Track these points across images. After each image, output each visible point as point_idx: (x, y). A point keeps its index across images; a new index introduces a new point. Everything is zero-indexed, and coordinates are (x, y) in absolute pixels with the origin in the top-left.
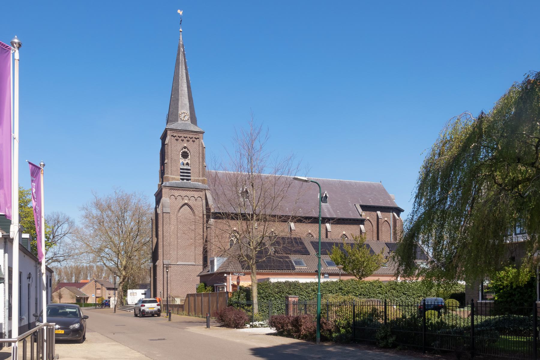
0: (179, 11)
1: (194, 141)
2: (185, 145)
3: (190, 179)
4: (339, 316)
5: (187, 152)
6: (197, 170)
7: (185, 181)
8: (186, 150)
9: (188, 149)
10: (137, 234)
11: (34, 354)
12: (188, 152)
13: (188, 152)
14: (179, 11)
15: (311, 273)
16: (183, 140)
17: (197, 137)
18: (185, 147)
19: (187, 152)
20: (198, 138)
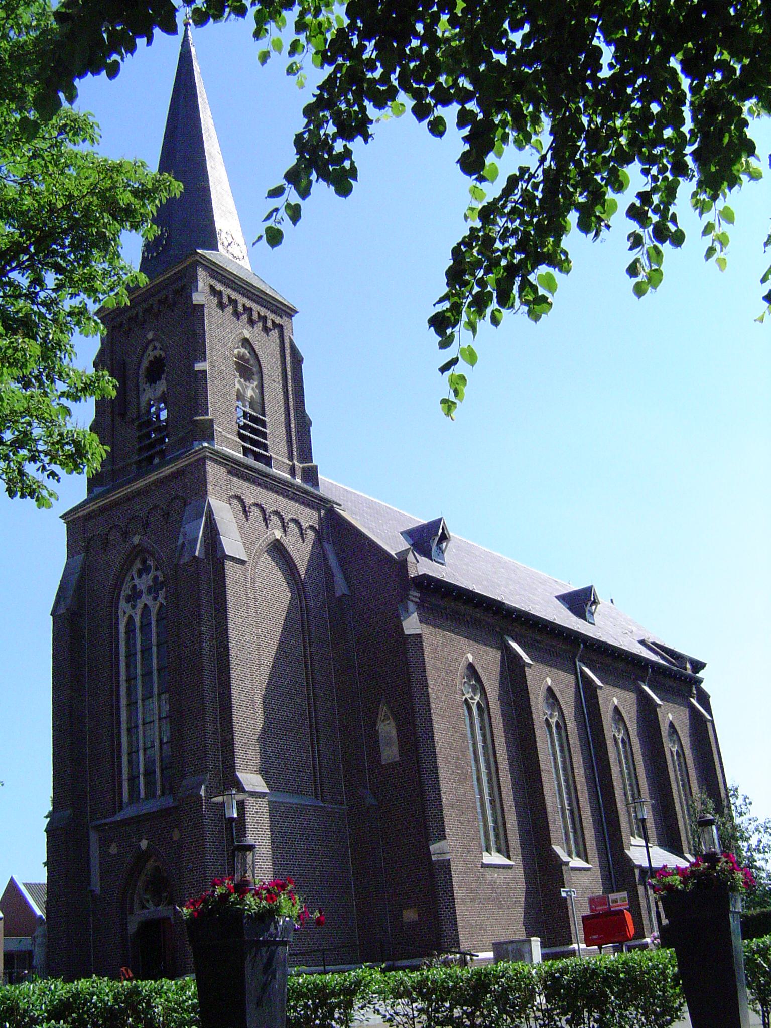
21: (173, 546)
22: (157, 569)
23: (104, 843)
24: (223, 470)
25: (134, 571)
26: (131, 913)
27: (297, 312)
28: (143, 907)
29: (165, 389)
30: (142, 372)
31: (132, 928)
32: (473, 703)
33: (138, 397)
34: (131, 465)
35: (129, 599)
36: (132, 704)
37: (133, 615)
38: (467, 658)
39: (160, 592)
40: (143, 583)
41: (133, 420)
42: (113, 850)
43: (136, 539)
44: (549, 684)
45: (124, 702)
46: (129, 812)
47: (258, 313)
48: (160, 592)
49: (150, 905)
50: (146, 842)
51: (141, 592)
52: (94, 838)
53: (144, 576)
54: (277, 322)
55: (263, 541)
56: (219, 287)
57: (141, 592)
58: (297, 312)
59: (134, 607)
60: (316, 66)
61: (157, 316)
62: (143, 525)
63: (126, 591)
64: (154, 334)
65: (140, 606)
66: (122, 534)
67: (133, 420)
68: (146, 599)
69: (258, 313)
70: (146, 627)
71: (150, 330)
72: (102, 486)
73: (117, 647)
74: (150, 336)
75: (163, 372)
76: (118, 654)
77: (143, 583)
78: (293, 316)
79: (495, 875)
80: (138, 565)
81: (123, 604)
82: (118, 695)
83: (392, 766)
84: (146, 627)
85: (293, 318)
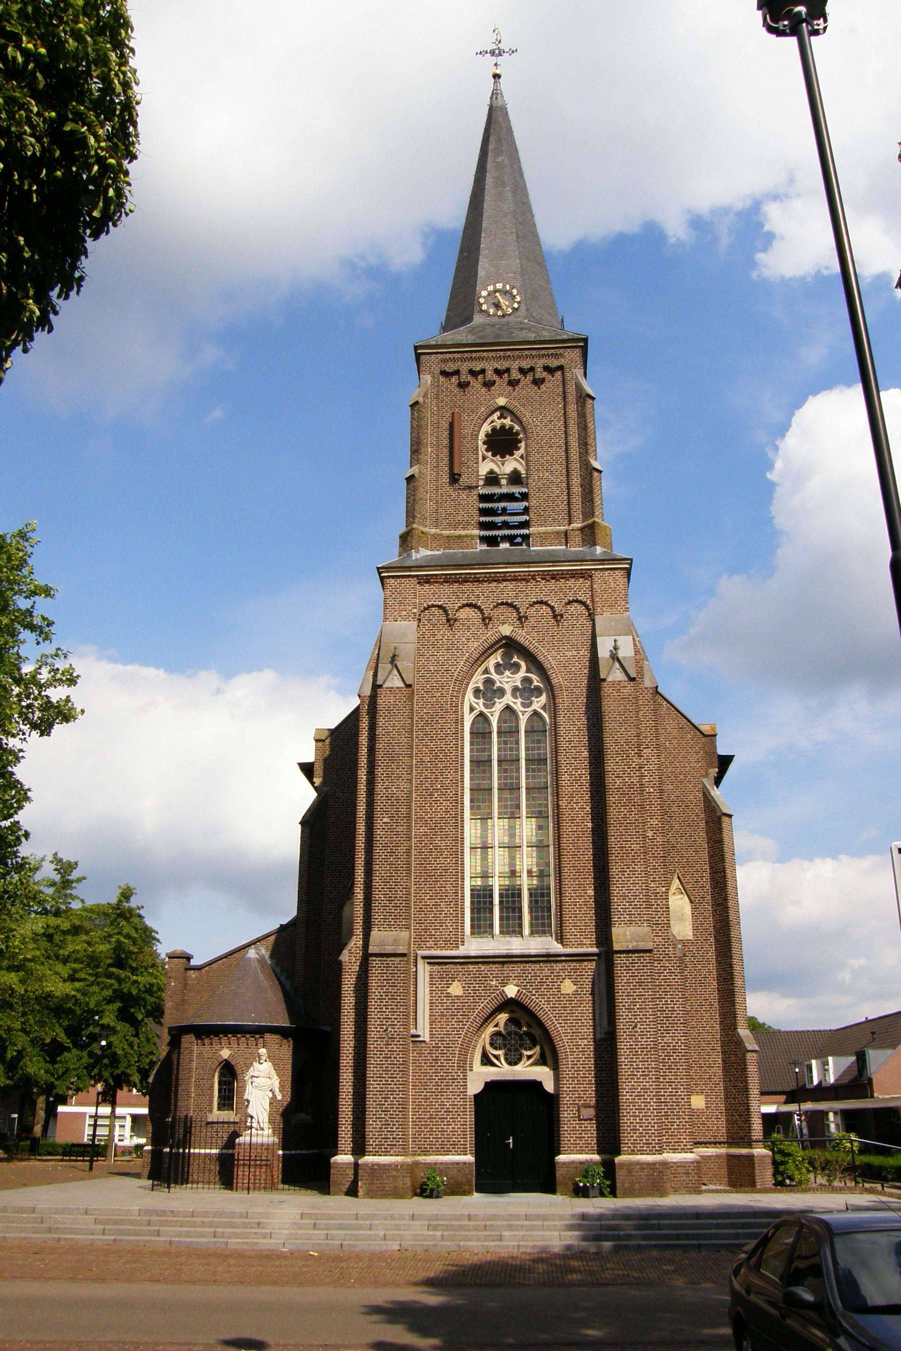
0: (93, 188)
1: (538, 382)
2: (501, 401)
3: (526, 538)
4: (636, 1027)
5: (512, 428)
6: (558, 491)
7: (504, 546)
8: (508, 422)
9: (517, 419)
10: (289, 1345)
11: (352, 1015)
12: (517, 428)
13: (517, 428)
14: (93, 188)
15: (248, 1033)
16: (488, 385)
17: (554, 363)
18: (504, 411)
19: (512, 428)
20: (561, 368)
23: (439, 982)
30: (482, 436)
46: (474, 946)
50: (517, 988)
63: (478, 680)
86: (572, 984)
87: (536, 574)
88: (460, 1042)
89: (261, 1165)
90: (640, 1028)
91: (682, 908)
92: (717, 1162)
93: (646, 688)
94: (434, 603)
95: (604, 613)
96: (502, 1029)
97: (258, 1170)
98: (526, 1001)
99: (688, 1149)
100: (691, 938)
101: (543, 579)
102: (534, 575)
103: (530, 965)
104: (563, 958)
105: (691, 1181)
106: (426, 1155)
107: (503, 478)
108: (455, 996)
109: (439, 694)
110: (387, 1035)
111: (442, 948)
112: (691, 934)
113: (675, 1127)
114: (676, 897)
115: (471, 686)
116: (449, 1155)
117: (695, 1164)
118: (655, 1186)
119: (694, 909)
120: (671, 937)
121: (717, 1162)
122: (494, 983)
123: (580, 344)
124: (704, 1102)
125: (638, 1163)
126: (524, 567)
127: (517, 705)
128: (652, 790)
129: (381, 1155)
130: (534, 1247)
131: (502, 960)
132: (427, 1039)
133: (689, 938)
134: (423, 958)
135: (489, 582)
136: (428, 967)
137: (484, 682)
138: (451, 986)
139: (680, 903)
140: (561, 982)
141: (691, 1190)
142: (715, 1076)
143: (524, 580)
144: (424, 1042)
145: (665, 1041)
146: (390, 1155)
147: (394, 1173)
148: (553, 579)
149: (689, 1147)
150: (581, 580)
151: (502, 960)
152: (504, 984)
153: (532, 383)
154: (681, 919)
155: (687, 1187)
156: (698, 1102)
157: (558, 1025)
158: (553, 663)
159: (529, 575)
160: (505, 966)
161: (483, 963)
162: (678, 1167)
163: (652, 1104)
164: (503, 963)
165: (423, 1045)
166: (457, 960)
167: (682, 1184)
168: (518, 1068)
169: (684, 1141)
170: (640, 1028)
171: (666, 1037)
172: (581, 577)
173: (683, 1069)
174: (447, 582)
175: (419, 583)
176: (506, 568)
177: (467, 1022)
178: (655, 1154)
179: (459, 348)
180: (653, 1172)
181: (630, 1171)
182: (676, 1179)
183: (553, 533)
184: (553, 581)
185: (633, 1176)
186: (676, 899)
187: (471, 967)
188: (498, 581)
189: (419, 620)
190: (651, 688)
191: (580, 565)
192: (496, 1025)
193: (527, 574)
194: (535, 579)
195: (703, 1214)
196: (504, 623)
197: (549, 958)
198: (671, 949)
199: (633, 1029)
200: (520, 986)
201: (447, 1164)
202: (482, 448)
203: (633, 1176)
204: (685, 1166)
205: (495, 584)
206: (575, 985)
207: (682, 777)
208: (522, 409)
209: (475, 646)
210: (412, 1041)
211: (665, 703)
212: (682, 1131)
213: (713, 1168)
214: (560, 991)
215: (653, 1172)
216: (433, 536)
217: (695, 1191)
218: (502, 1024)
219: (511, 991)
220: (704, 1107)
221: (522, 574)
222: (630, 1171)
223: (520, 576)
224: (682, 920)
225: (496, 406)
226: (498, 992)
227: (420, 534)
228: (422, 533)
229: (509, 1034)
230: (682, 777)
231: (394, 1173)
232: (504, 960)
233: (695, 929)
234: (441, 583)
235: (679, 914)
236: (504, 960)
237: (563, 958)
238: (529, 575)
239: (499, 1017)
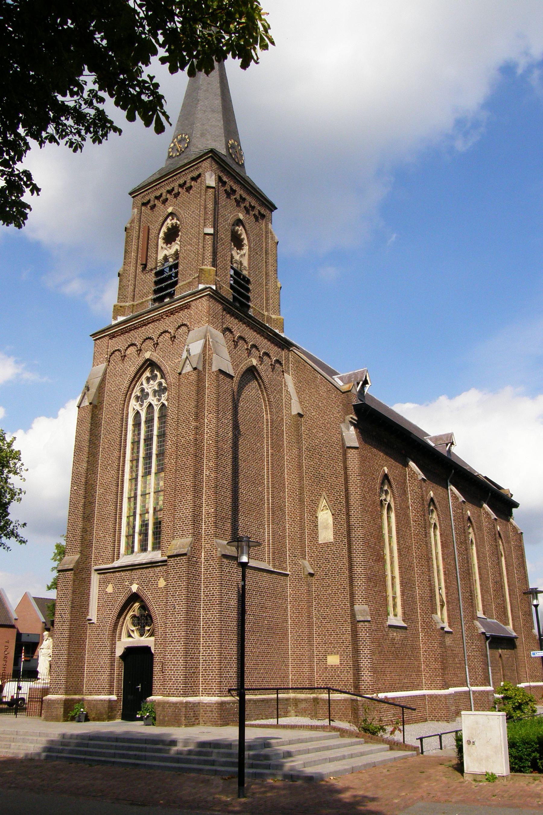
21: (177, 361)
22: (162, 378)
23: (103, 584)
24: (220, 307)
25: (143, 379)
26: (120, 639)
27: (276, 208)
28: (130, 636)
29: (179, 249)
30: (162, 235)
31: (119, 651)
32: (386, 504)
33: (157, 253)
34: (147, 301)
35: (137, 398)
36: (134, 479)
37: (140, 411)
38: (384, 470)
39: (163, 395)
40: (150, 387)
41: (152, 270)
42: (110, 589)
43: (147, 355)
44: (432, 496)
45: (127, 476)
46: (124, 560)
47: (250, 203)
48: (163, 395)
49: (136, 635)
50: (137, 586)
51: (148, 394)
52: (95, 578)
53: (151, 382)
54: (262, 213)
55: (244, 365)
56: (225, 179)
57: (148, 394)
58: (276, 208)
59: (141, 405)
60: (28, 592)
61: (177, 195)
62: (154, 344)
63: (137, 392)
64: (174, 208)
65: (146, 404)
66: (137, 351)
67: (152, 270)
68: (152, 399)
69: (250, 203)
70: (150, 421)
71: (171, 206)
72: (124, 315)
73: (126, 435)
74: (170, 210)
75: (178, 236)
76: (125, 440)
77: (150, 387)
78: (273, 211)
79: (394, 634)
80: (147, 374)
81: (133, 402)
82: (123, 471)
83: (327, 545)
84: (150, 421)
85: (273, 213)
86: (164, 581)
87: (163, 314)
88: (109, 623)
89: (37, 701)
90: (178, 609)
91: (327, 520)
92: (345, 705)
93: (213, 372)
94: (116, 349)
95: (195, 328)
96: (136, 614)
97: (36, 704)
98: (141, 594)
99: (216, 694)
100: (332, 541)
101: (167, 316)
102: (162, 315)
103: (144, 570)
104: (160, 564)
105: (213, 716)
106: (91, 695)
107: (170, 258)
108: (109, 593)
109: (114, 405)
110: (62, 619)
111: (105, 563)
112: (332, 538)
113: (210, 678)
114: (324, 512)
115: (133, 395)
116: (100, 695)
117: (217, 705)
118: (176, 719)
119: (335, 519)
120: (215, 543)
121: (345, 705)
122: (127, 583)
123: (209, 155)
124: (339, 660)
125: (168, 703)
126: (157, 312)
127: (154, 402)
128: (211, 442)
129: (54, 694)
130: (13, 753)
131: (130, 568)
132: (95, 622)
133: (331, 541)
134: (96, 570)
135: (141, 327)
136: (99, 576)
137: (141, 391)
138: (108, 587)
139: (325, 516)
140: (159, 580)
141: (214, 723)
142: (346, 640)
143: (157, 320)
144: (93, 623)
145: (208, 617)
146: (59, 694)
147: (57, 706)
148: (171, 314)
149: (217, 692)
150: (186, 310)
151: (130, 568)
152: (131, 584)
153: (186, 192)
154: (326, 528)
155: (211, 721)
156: (333, 660)
157: (156, 609)
158: (169, 369)
159: (159, 316)
160: (133, 572)
161: (122, 571)
162: (207, 706)
163: (181, 661)
164: (132, 570)
165: (94, 625)
166: (110, 571)
167: (209, 719)
168: (143, 638)
169: (215, 688)
170: (178, 609)
171: (208, 614)
172: (186, 308)
173: (216, 637)
174: (122, 334)
175: (110, 339)
176: (148, 315)
177: (113, 609)
178: (180, 697)
179: (150, 185)
180: (176, 709)
181: (163, 708)
182: (205, 715)
183: (186, 284)
184: (172, 316)
185: (165, 711)
186: (323, 514)
187: (117, 574)
188: (145, 325)
189: (109, 361)
190: (216, 372)
191: (184, 301)
192: (134, 611)
193: (158, 316)
194: (162, 318)
195: (120, 738)
196: (147, 351)
197: (152, 564)
198: (214, 552)
199: (174, 609)
200: (139, 584)
201: (97, 701)
202: (161, 242)
203: (165, 711)
204: (211, 706)
205: (144, 327)
206: (165, 581)
207: (329, 425)
208: (179, 210)
209: (133, 370)
210: (89, 623)
211: (320, 375)
212: (214, 680)
213: (342, 709)
214: (157, 586)
215: (176, 709)
216: (128, 307)
217: (215, 724)
218: (136, 610)
219: (134, 588)
220: (339, 664)
221: (156, 317)
222: (163, 708)
223: (155, 318)
224: (326, 528)
225: (167, 214)
226: (128, 589)
227: (119, 308)
228: (121, 307)
229: (141, 615)
230: (329, 425)
231: (57, 706)
232: (132, 568)
233: (335, 534)
234: (120, 335)
235: (325, 524)
236: (132, 568)
237: (160, 564)
238: (159, 316)
239: (135, 605)
